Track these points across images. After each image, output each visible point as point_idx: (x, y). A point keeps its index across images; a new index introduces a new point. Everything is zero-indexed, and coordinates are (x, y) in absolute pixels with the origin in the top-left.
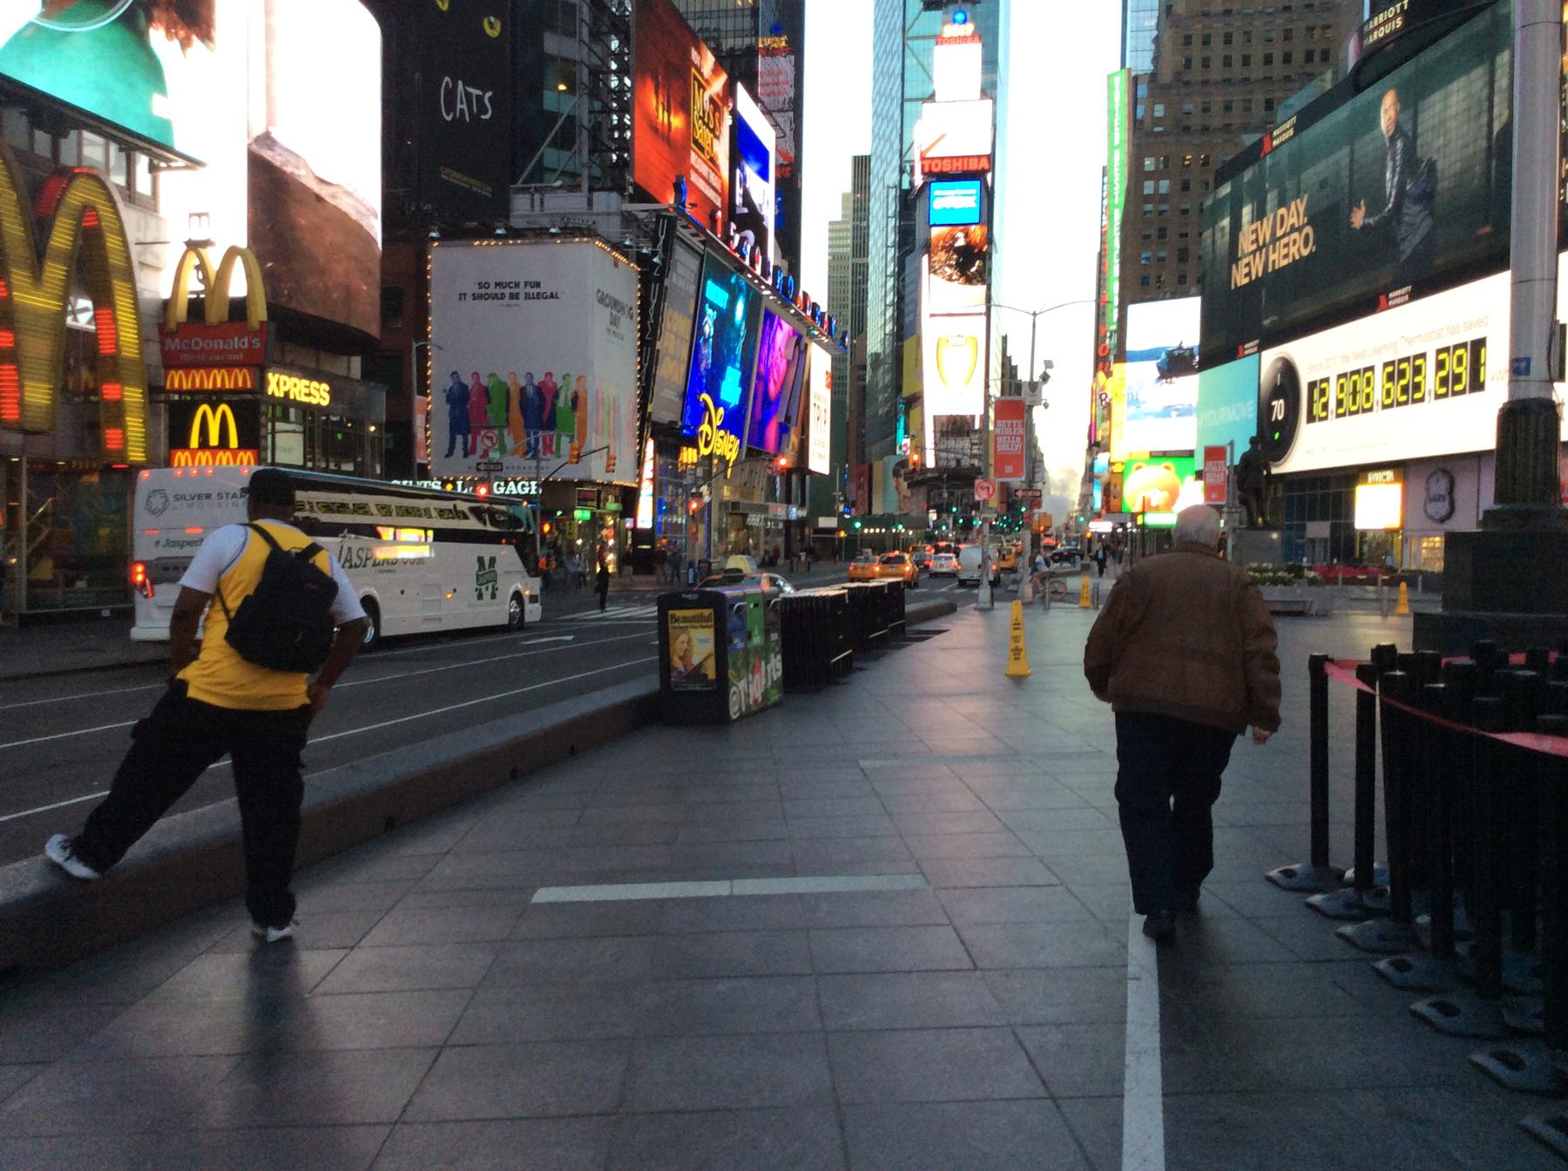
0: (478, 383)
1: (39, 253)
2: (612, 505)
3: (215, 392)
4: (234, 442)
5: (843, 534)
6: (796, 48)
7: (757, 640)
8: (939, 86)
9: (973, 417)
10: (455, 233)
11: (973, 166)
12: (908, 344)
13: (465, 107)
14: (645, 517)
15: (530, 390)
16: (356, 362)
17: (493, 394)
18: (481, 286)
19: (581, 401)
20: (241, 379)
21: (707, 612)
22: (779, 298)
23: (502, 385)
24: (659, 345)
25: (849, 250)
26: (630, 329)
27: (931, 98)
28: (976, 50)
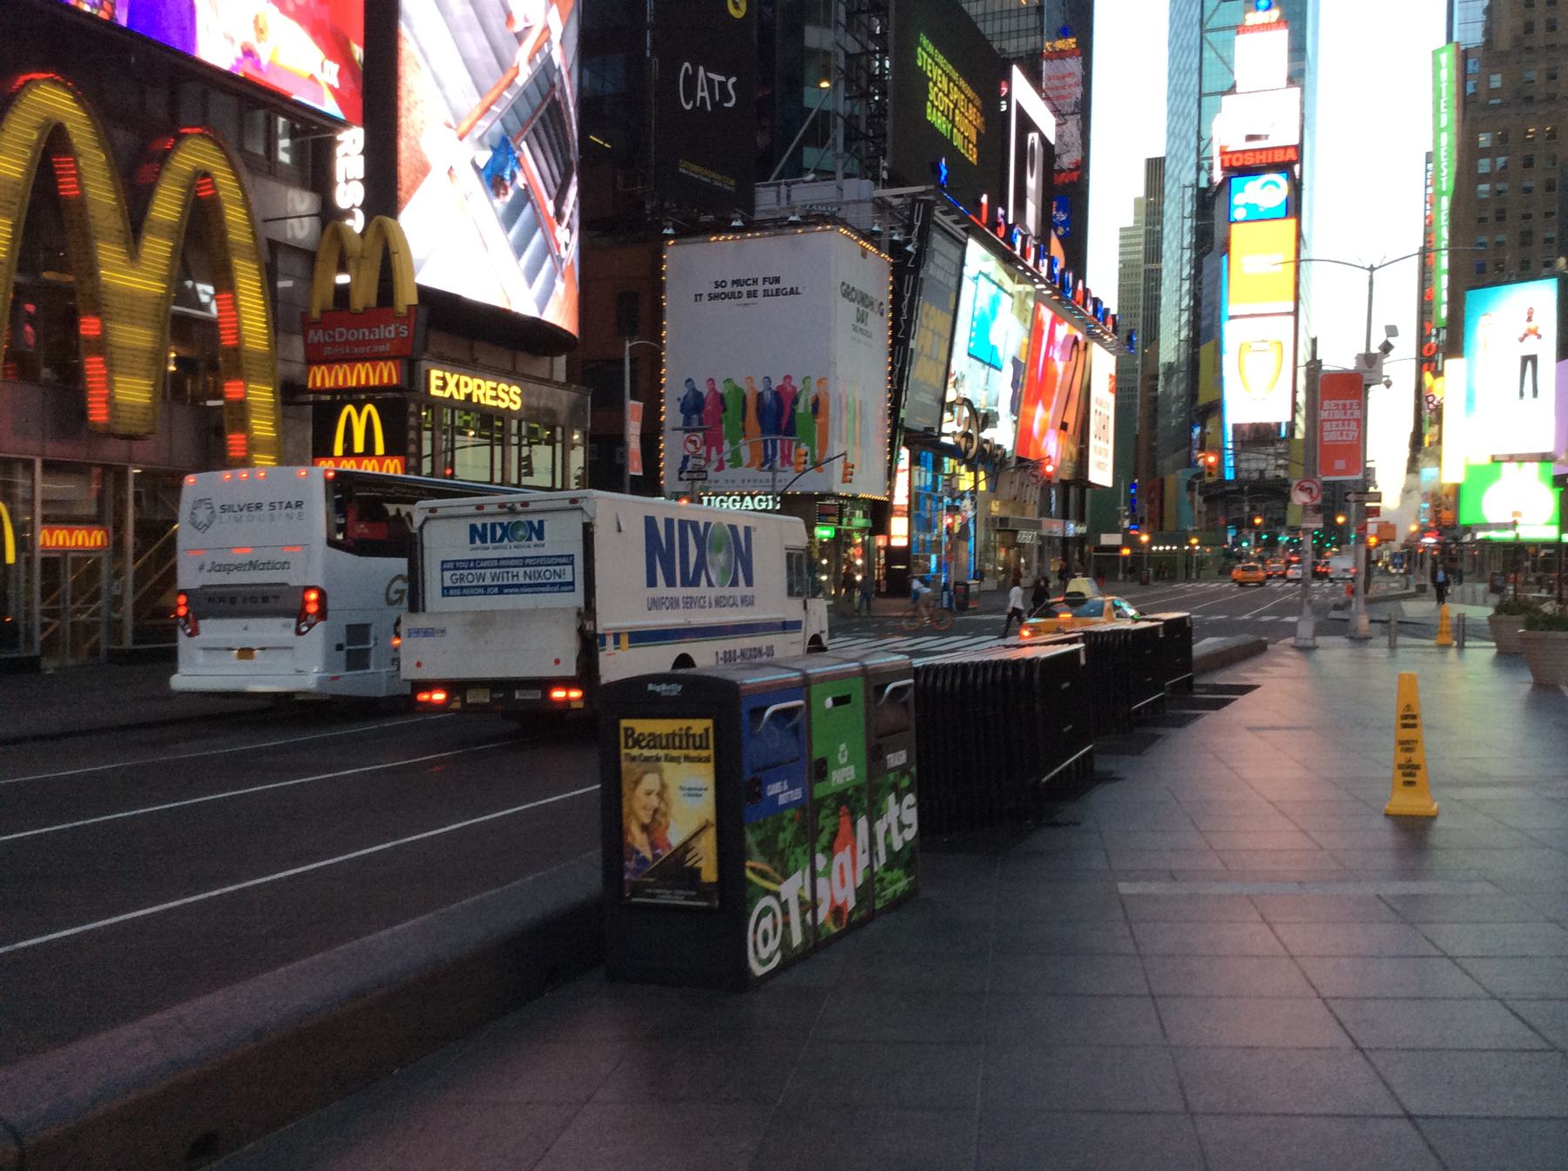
0: (713, 390)
1: (135, 224)
2: (859, 521)
3: (359, 389)
4: (380, 448)
5: (1126, 552)
6: (1085, 50)
7: (844, 774)
8: (1242, 76)
9: (1279, 425)
10: (691, 230)
11: (1279, 157)
12: (1205, 350)
13: (706, 94)
14: (899, 531)
15: (768, 396)
16: (561, 362)
17: (729, 402)
18: (717, 285)
19: (821, 409)
20: (386, 373)
21: (699, 726)
22: (1055, 292)
23: (738, 390)
24: (912, 344)
25: (1141, 256)
26: (880, 326)
27: (1232, 90)
28: (1282, 37)
